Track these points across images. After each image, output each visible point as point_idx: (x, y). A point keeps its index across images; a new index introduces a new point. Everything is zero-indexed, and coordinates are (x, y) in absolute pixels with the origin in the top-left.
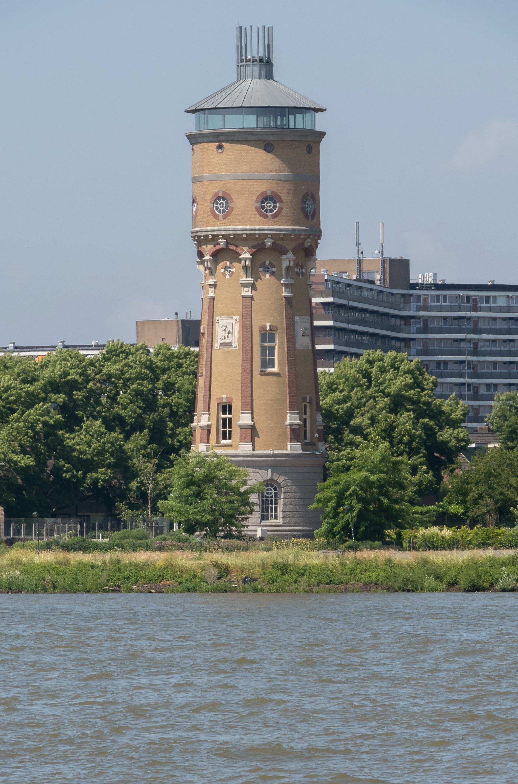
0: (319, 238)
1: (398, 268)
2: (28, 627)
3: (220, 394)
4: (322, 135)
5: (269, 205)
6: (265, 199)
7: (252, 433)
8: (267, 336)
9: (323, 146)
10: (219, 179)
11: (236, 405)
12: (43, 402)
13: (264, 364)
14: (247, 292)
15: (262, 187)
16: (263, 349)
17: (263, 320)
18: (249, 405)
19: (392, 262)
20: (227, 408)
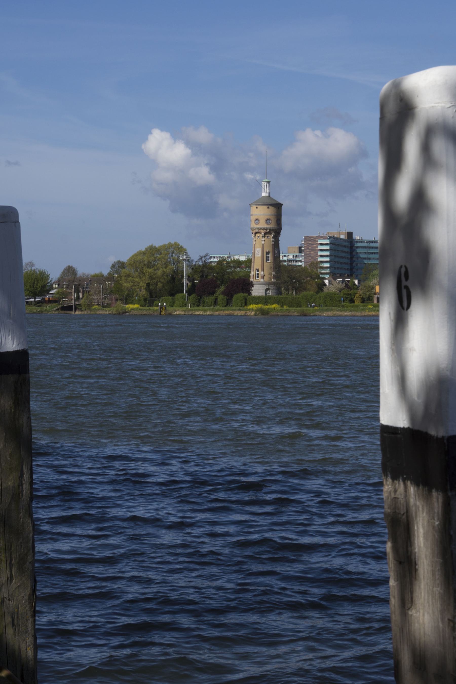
0: (179, 245)
1: (350, 234)
2: (305, 386)
3: (256, 267)
4: (282, 205)
5: (268, 221)
6: (267, 220)
7: (263, 277)
8: (268, 253)
9: (283, 207)
10: (256, 215)
11: (260, 270)
12: (319, 276)
13: (267, 260)
14: (263, 243)
15: (267, 217)
16: (267, 257)
17: (267, 249)
18: (263, 270)
19: (348, 233)
20: (258, 270)
